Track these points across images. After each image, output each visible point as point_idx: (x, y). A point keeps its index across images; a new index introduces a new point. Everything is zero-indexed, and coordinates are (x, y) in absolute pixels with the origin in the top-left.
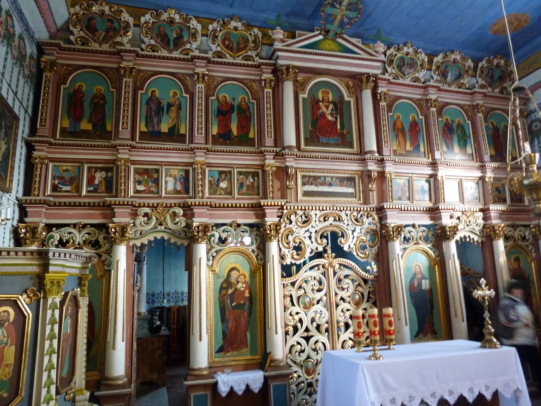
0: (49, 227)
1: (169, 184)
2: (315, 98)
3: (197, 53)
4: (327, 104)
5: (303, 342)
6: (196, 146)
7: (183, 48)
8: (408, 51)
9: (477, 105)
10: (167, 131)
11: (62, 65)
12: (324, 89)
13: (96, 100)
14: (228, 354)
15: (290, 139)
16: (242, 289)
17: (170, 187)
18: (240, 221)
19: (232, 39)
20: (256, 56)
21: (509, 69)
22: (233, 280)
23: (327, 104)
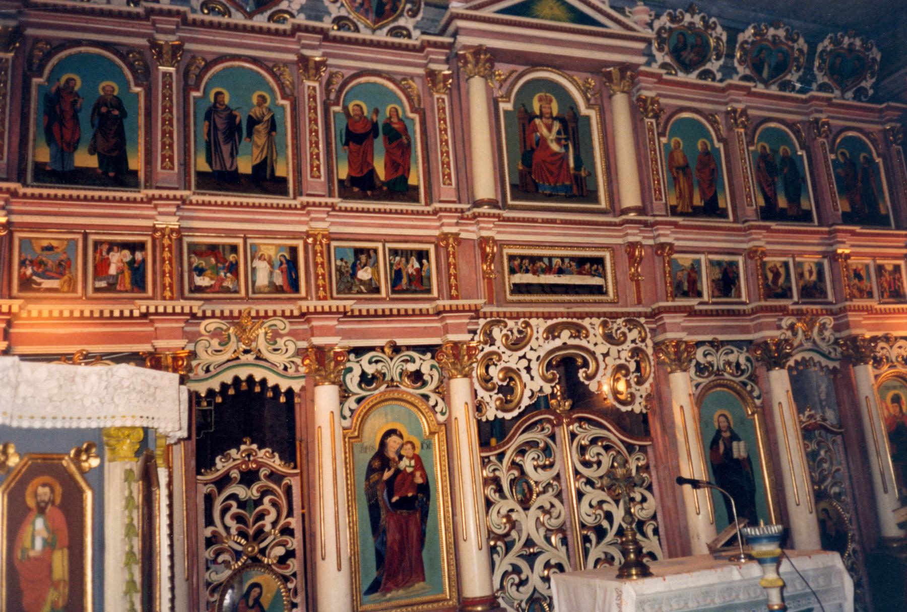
2: (526, 111)
3: (301, 20)
5: (523, 565)
6: (311, 200)
7: (274, 9)
8: (692, 20)
9: (817, 121)
11: (37, 40)
12: (542, 94)
13: (104, 110)
14: (389, 595)
16: (409, 470)
17: (262, 279)
18: (400, 342)
20: (415, 27)
21: (871, 56)
22: (391, 454)
23: (550, 121)
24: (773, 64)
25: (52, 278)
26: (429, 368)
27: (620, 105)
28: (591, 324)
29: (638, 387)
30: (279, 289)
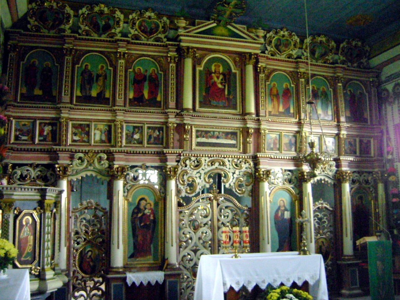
0: (14, 166)
1: (96, 135)
2: (208, 71)
8: (284, 34)
13: (45, 73)
14: (137, 259)
15: (188, 103)
16: (148, 214)
17: (98, 138)
22: (142, 207)
23: (218, 75)
25: (26, 136)
27: (250, 69)
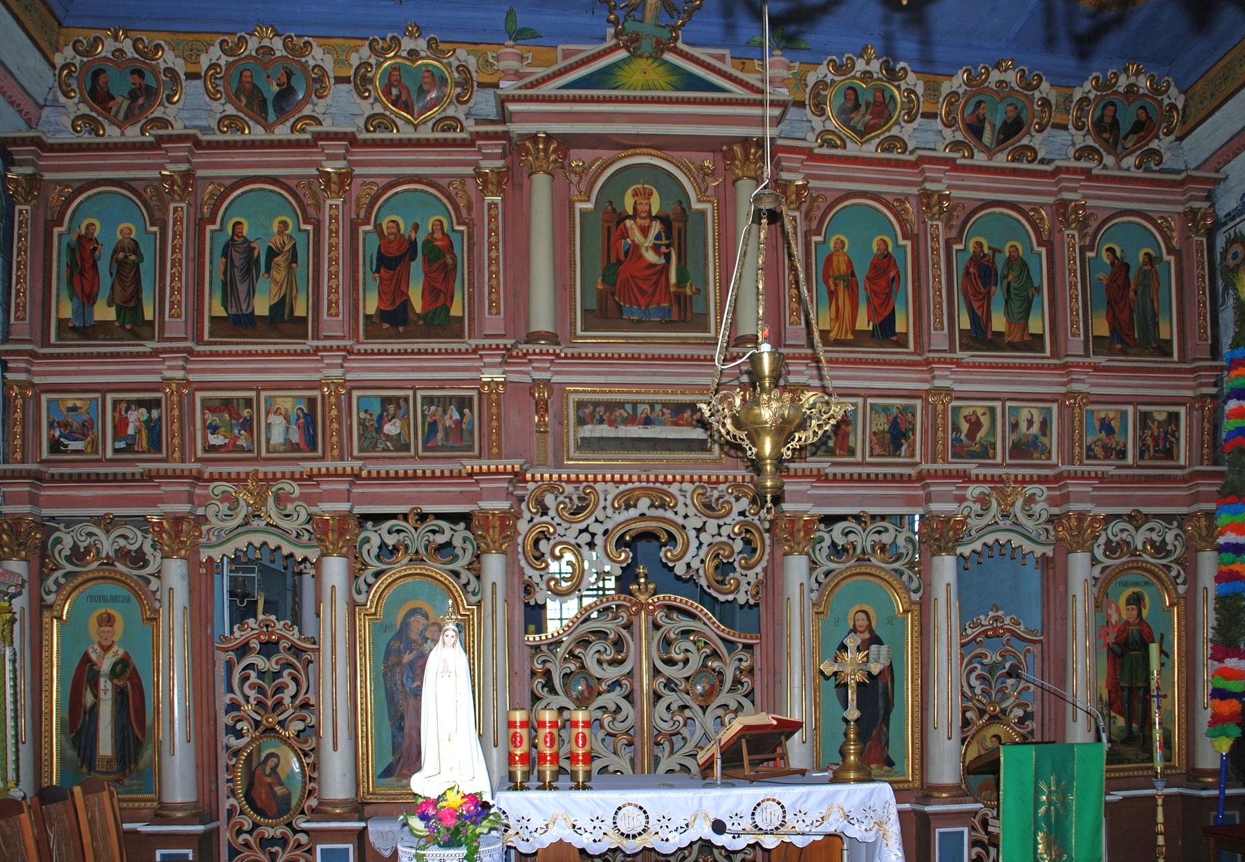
2: (614, 210)
4: (646, 223)
8: (868, 68)
10: (266, 312)
17: (277, 437)
18: (427, 509)
19: (405, 81)
21: (1166, 101)
22: (414, 635)
23: (646, 223)
24: (998, 124)
26: (461, 541)
28: (681, 490)
29: (744, 572)
30: (295, 447)
